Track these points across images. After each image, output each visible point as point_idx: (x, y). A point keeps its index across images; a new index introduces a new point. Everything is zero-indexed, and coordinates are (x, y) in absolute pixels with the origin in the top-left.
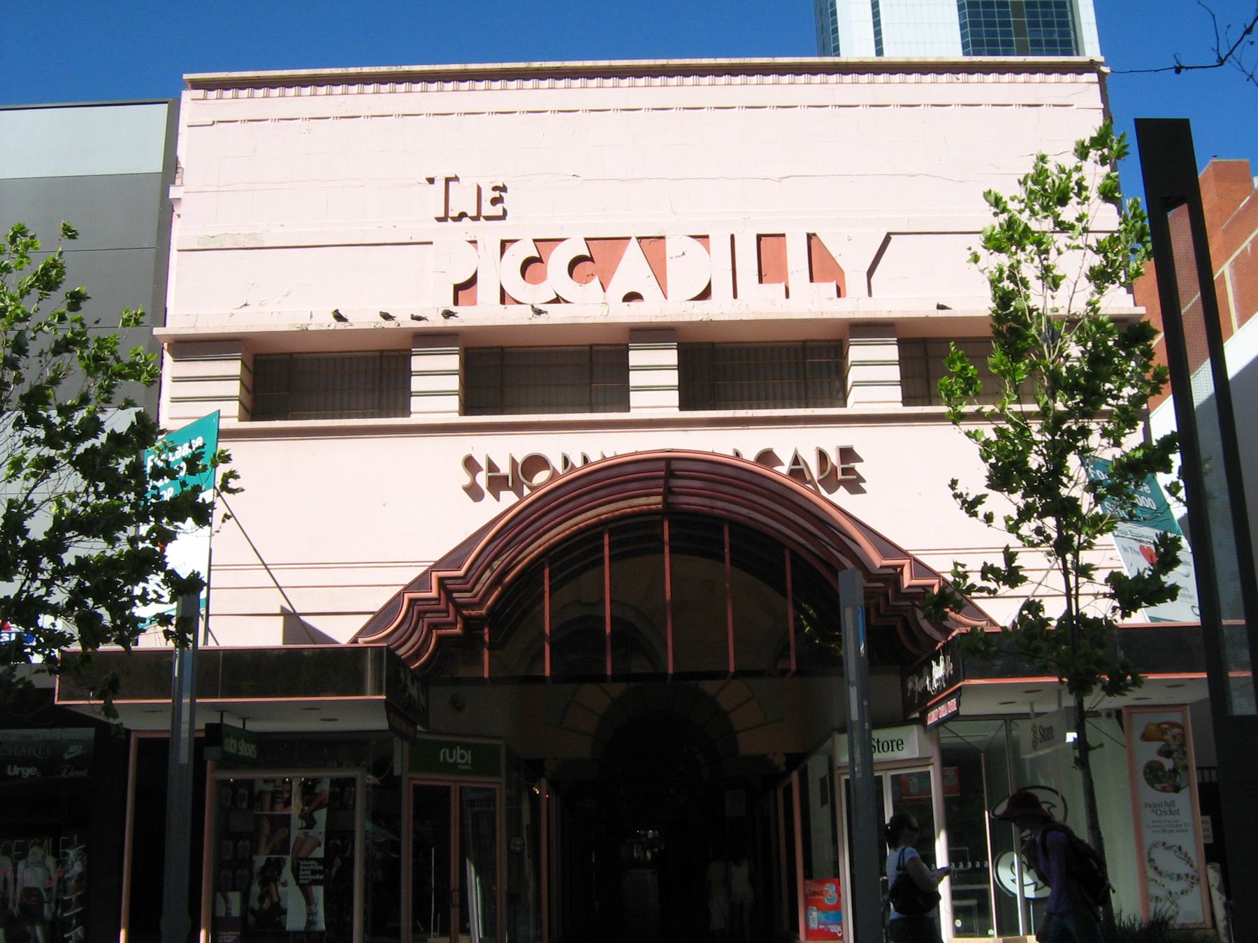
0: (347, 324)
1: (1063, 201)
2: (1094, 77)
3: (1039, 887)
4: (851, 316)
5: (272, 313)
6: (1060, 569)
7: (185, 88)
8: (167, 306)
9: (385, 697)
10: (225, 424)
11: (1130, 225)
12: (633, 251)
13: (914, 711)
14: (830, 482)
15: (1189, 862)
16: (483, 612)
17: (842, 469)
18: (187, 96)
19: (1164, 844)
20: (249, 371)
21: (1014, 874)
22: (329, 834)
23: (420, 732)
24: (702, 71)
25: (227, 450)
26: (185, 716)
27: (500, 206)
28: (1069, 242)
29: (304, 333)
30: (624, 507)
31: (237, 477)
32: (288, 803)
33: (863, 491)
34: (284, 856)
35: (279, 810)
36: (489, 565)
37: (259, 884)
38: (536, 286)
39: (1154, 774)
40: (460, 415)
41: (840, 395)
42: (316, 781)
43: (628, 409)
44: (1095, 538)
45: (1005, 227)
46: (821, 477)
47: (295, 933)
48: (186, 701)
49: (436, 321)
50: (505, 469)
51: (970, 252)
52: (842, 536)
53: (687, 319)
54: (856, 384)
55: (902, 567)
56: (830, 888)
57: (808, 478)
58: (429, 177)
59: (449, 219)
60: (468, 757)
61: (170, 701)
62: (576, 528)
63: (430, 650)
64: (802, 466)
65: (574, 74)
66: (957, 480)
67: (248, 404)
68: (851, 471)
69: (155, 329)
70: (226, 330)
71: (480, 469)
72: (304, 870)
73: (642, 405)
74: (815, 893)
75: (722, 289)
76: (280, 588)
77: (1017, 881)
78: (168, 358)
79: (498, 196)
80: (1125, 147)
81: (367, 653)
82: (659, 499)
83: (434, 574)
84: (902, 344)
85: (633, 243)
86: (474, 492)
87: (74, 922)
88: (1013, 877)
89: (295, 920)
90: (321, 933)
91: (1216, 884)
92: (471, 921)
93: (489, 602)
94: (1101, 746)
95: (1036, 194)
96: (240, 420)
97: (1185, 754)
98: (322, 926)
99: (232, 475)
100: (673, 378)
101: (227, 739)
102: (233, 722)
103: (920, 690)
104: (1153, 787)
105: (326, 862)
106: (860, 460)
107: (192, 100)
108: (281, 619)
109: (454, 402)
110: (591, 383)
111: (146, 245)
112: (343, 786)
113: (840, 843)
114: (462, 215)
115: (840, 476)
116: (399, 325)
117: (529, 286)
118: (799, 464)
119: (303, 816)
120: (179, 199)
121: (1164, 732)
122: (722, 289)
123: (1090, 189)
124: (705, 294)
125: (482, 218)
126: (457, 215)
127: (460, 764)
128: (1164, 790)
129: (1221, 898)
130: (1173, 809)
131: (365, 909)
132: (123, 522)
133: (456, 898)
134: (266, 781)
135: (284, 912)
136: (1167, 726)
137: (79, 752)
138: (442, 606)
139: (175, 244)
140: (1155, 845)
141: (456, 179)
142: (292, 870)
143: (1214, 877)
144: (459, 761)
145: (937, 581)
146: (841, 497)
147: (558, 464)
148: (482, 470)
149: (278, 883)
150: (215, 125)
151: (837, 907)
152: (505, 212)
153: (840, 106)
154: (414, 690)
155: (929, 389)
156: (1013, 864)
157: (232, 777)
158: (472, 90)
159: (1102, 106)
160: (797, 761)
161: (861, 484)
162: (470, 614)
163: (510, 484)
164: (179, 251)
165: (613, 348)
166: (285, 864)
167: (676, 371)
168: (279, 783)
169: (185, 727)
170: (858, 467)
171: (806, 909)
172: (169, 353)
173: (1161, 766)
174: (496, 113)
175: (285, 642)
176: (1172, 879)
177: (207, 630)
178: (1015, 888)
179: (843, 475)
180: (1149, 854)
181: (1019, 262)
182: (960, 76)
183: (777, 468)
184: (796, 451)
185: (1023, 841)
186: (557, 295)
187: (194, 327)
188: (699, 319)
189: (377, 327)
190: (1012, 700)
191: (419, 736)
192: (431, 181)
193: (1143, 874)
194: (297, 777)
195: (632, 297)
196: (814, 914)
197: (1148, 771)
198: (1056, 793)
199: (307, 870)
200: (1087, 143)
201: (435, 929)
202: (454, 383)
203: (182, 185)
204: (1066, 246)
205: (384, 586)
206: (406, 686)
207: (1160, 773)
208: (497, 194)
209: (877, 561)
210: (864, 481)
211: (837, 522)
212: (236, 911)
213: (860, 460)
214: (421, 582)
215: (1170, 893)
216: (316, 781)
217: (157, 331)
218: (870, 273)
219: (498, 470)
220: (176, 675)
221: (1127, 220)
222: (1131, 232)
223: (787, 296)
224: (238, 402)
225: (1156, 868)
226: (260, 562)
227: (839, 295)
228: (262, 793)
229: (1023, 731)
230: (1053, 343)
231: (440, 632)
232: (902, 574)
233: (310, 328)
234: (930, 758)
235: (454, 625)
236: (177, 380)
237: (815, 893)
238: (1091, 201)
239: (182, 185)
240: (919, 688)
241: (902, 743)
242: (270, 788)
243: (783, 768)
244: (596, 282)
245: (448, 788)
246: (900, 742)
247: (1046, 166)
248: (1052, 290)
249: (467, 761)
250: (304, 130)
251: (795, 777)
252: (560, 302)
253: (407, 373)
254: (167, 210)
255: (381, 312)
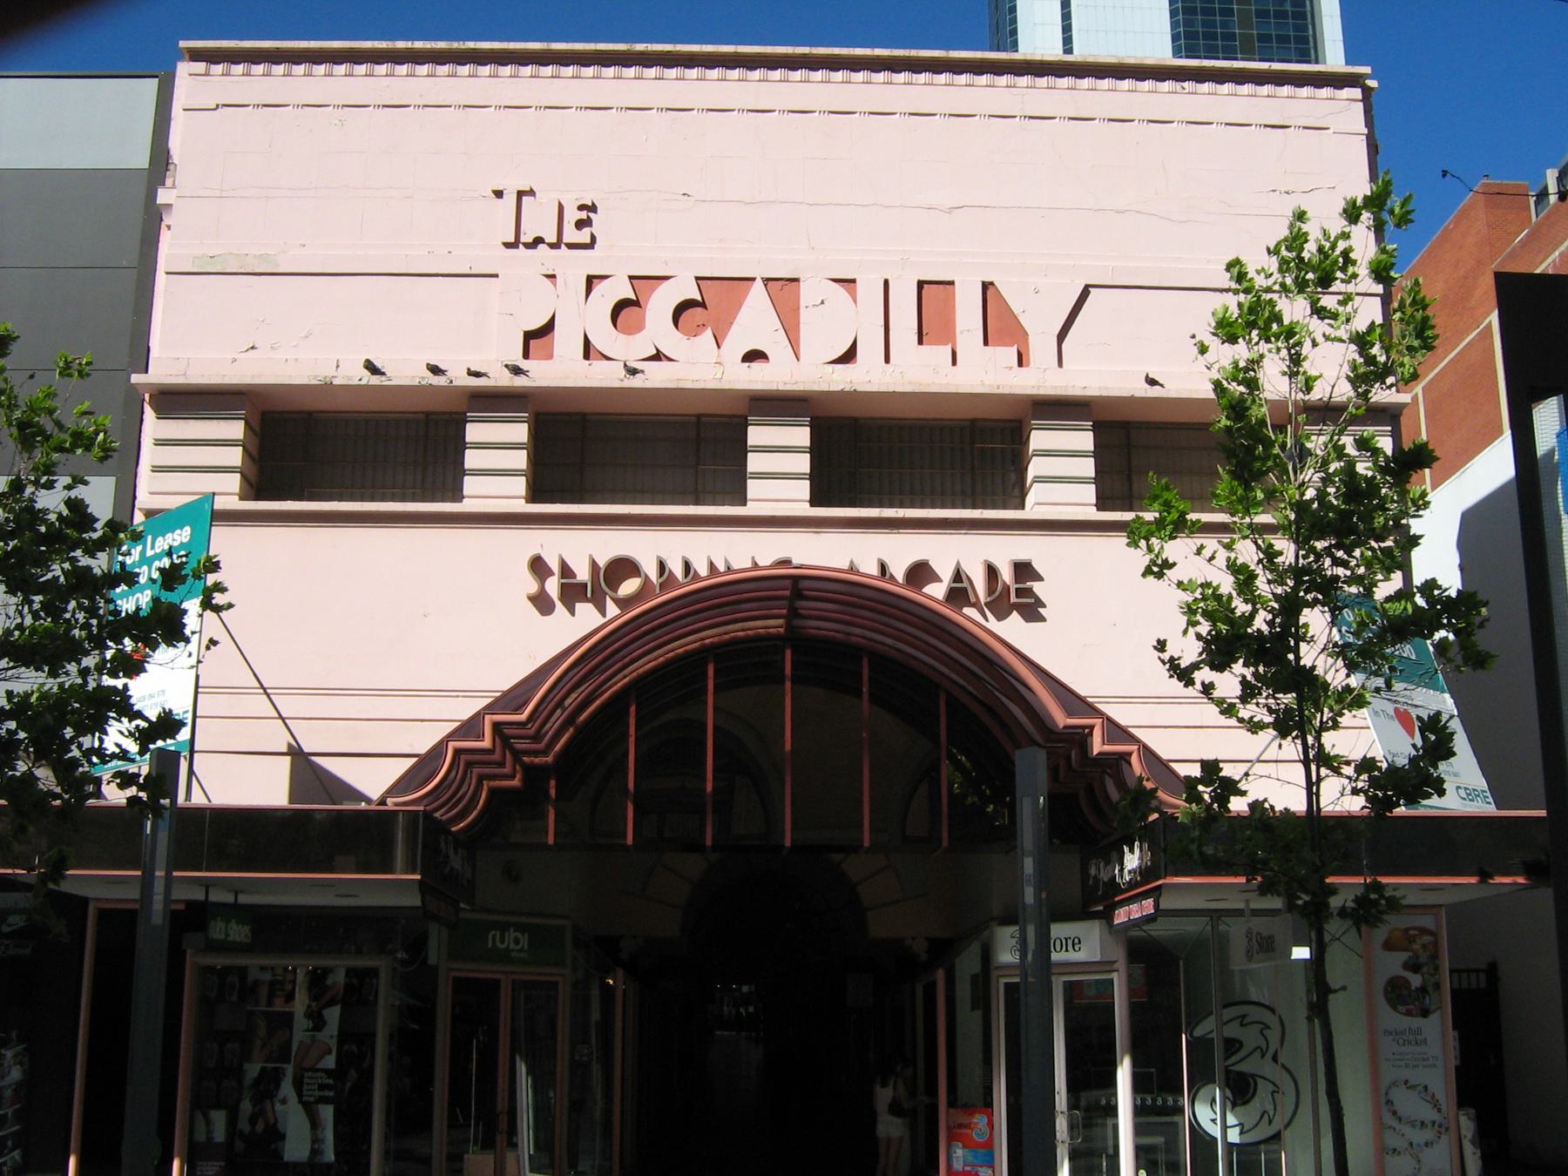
0: (383, 378)
1: (1325, 281)
2: (1357, 93)
3: (1245, 1129)
4: (1034, 392)
5: (287, 360)
6: (1300, 761)
7: (182, 59)
8: (150, 345)
9: (419, 877)
10: (221, 503)
11: (1409, 313)
12: (757, 296)
13: (1096, 904)
14: (1000, 606)
15: (1436, 1106)
16: (549, 759)
17: (1017, 589)
18: (184, 69)
19: (1406, 1082)
20: (256, 434)
21: (1215, 1113)
22: (343, 1038)
23: (464, 909)
24: (854, 65)
25: (216, 556)
26: (159, 887)
27: (587, 231)
28: (1329, 331)
29: (327, 388)
30: (737, 631)
31: (223, 590)
32: (290, 997)
33: (1042, 619)
34: (285, 1066)
35: (279, 1006)
36: (560, 704)
37: (251, 1101)
38: (631, 336)
39: (1397, 993)
40: (527, 502)
41: (1017, 492)
42: (326, 971)
43: (743, 502)
44: (1341, 715)
45: (1245, 309)
46: (989, 599)
47: (296, 1164)
48: (160, 873)
49: (503, 379)
50: (583, 574)
51: (1194, 341)
52: (1013, 681)
53: (825, 388)
54: (1039, 479)
55: (1092, 728)
56: (980, 1120)
57: (973, 599)
58: (496, 189)
59: (521, 245)
60: (524, 941)
61: (139, 873)
62: (672, 654)
63: (479, 807)
64: (965, 584)
65: (689, 61)
66: (1165, 641)
67: (252, 477)
68: (1029, 592)
69: (133, 375)
70: (227, 381)
71: (551, 573)
72: (308, 1084)
73: (762, 497)
74: (960, 1126)
75: (870, 350)
76: (283, 719)
77: (1218, 1122)
78: (149, 413)
79: (585, 217)
80: (1408, 212)
81: (398, 815)
82: (781, 621)
83: (487, 717)
84: (1099, 429)
85: (758, 286)
86: (542, 603)
87: (10, 1143)
88: (1214, 1117)
89: (296, 1149)
90: (329, 1166)
91: (1470, 1135)
92: (520, 1136)
93: (557, 748)
94: (1344, 988)
95: (1289, 263)
96: (241, 499)
97: (1437, 968)
98: (330, 1156)
99: (219, 588)
100: (803, 463)
101: (213, 922)
102: (217, 896)
103: (1105, 879)
104: (1395, 1008)
105: (338, 1074)
106: (1039, 578)
107: (191, 75)
108: (288, 759)
109: (519, 485)
110: (698, 464)
111: (125, 263)
112: (361, 981)
113: (995, 1063)
114: (538, 241)
115: (1013, 599)
116: (451, 382)
117: (622, 336)
118: (962, 582)
119: (309, 1015)
120: (169, 206)
121: (1412, 940)
122: (870, 350)
123: (1359, 262)
124: (849, 356)
125: (563, 246)
126: (531, 241)
127: (513, 950)
128: (1409, 1013)
129: (1474, 1153)
130: (1419, 1038)
131: (386, 1133)
132: (74, 651)
133: (503, 1123)
134: (263, 968)
135: (282, 1137)
136: (1416, 932)
137: (22, 924)
138: (497, 756)
139: (162, 265)
140: (1394, 1084)
141: (531, 193)
142: (294, 1084)
143: (1467, 1126)
144: (512, 946)
145: (1136, 747)
146: (1013, 630)
147: (652, 571)
148: (553, 574)
149: (275, 1099)
150: (219, 110)
151: (989, 1145)
152: (593, 238)
153: (1031, 117)
154: (456, 862)
155: (1131, 489)
156: (1214, 1100)
157: (219, 961)
158: (556, 77)
159: (1366, 131)
160: (943, 950)
161: (1040, 610)
162: (532, 762)
163: (589, 595)
164: (167, 273)
165: (726, 420)
166: (284, 1075)
167: (808, 455)
168: (279, 971)
169: (158, 898)
170: (1037, 587)
171: (949, 1146)
172: (151, 406)
173: (1407, 982)
174: (586, 108)
175: (292, 800)
176: (1414, 1126)
177: (191, 772)
178: (1216, 1131)
179: (1017, 597)
180: (1386, 1094)
181: (1262, 356)
182: (1186, 84)
183: (929, 589)
184: (958, 563)
185: (1228, 1072)
186: (657, 349)
187: (185, 374)
188: (839, 388)
189: (424, 383)
190: (1225, 897)
191: (461, 915)
192: (499, 194)
193: (1378, 1119)
194: (301, 966)
195: (754, 356)
196: (959, 1152)
197: (1389, 989)
198: (1273, 1011)
199: (314, 1084)
200: (1359, 202)
201: (475, 1143)
202: (520, 460)
203: (174, 186)
204: (1324, 335)
205: (422, 721)
206: (447, 856)
207: (1405, 992)
208: (583, 215)
209: (1061, 719)
210: (1044, 606)
211: (1006, 662)
212: (220, 1135)
213: (1039, 578)
214: (469, 728)
215: (1411, 1144)
216: (326, 971)
217: (136, 378)
218: (1062, 336)
219: (573, 575)
220: (148, 832)
221: (1404, 307)
222: (1408, 324)
223: (954, 362)
224: (239, 475)
225: (1395, 1113)
226: (258, 686)
227: (1020, 364)
228: (256, 983)
229: (1236, 931)
230: (1300, 462)
231: (494, 784)
232: (1092, 735)
233: (336, 382)
234: (1115, 962)
235: (513, 777)
236: (160, 443)
237: (960, 1126)
238: (1358, 280)
239: (174, 186)
240: (1104, 876)
241: (1080, 942)
242: (267, 976)
243: (924, 957)
244: (708, 335)
245: (497, 982)
246: (1076, 941)
247: (1305, 228)
248: (1303, 392)
249: (523, 947)
250: (337, 121)
251: (940, 975)
252: (660, 360)
253: (460, 445)
254: (153, 218)
255: (428, 364)
